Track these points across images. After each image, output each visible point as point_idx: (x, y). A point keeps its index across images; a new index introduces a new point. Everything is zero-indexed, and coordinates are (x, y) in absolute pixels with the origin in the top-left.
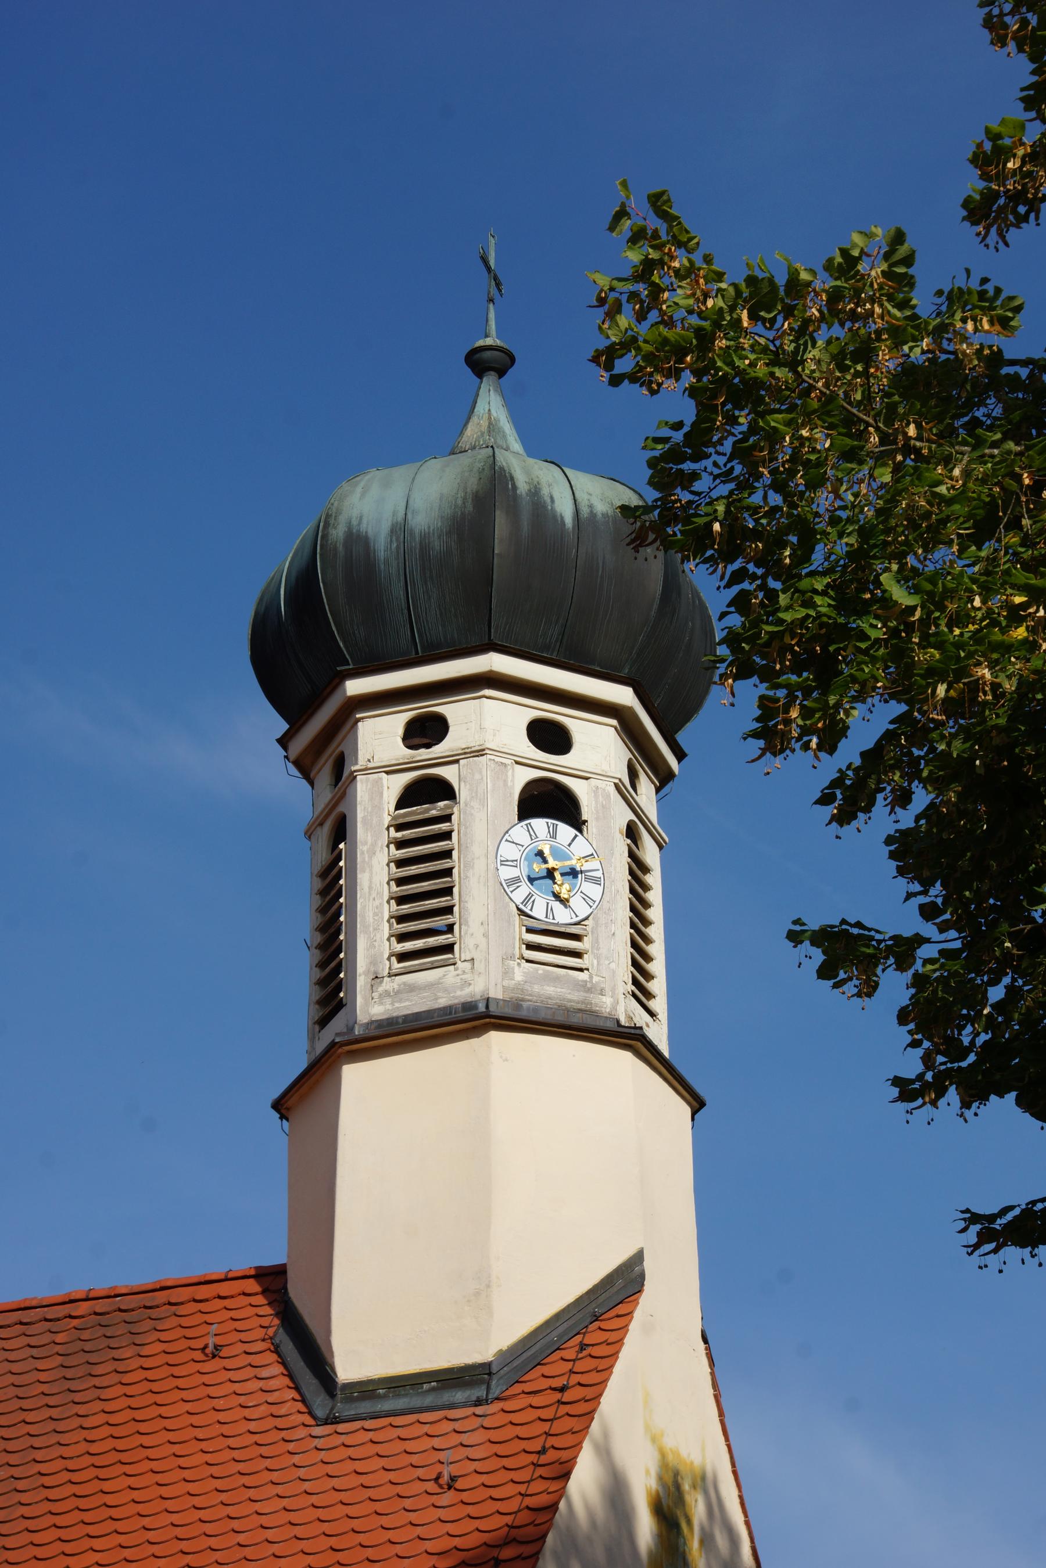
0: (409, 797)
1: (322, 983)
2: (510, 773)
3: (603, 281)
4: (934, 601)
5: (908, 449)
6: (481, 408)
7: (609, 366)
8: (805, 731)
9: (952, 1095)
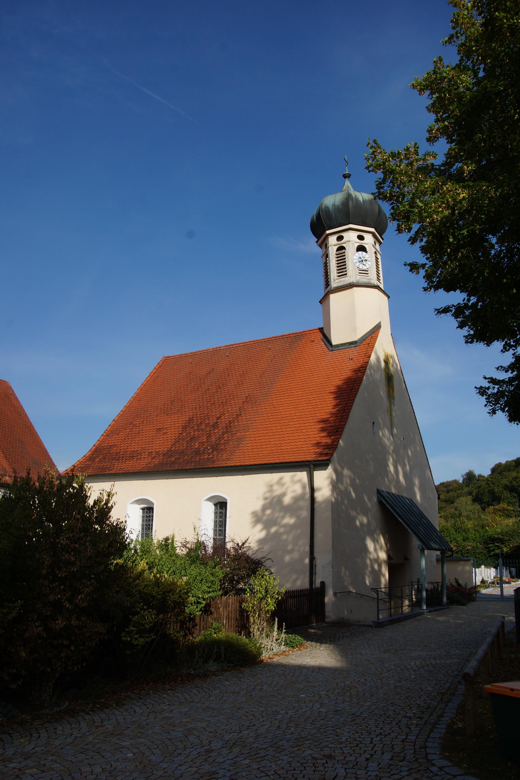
0: (338, 250)
1: (326, 281)
3: (366, 155)
4: (426, 205)
5: (420, 180)
6: (346, 184)
7: (368, 169)
8: (405, 229)
9: (433, 289)
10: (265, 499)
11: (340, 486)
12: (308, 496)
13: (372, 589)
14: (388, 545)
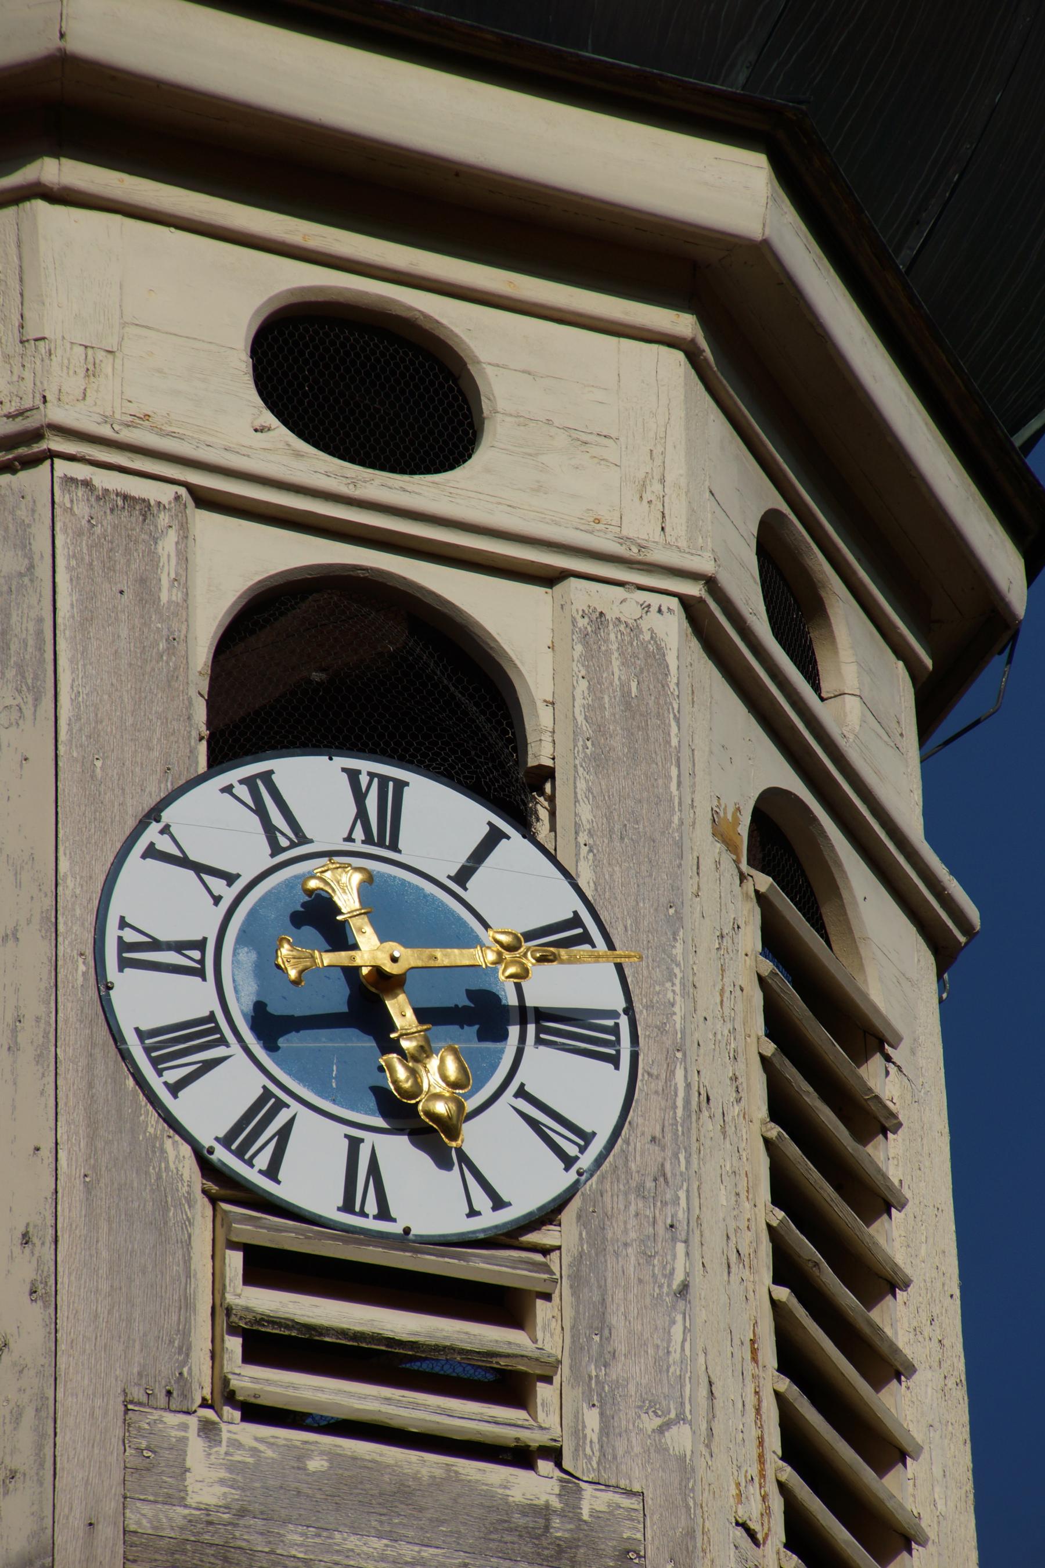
2: (168, 545)
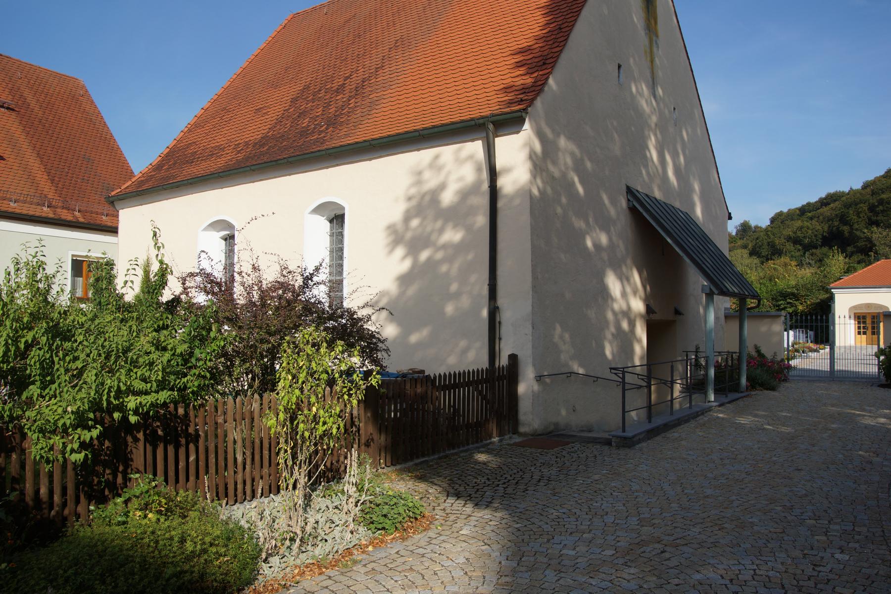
10: (409, 199)
11: (551, 167)
12: (486, 186)
13: (611, 369)
14: (648, 288)
